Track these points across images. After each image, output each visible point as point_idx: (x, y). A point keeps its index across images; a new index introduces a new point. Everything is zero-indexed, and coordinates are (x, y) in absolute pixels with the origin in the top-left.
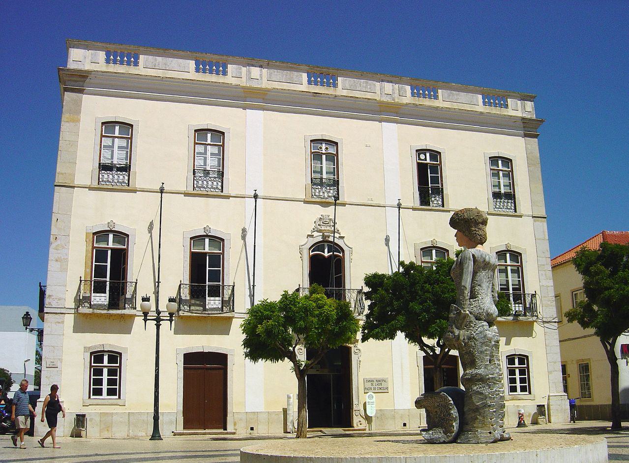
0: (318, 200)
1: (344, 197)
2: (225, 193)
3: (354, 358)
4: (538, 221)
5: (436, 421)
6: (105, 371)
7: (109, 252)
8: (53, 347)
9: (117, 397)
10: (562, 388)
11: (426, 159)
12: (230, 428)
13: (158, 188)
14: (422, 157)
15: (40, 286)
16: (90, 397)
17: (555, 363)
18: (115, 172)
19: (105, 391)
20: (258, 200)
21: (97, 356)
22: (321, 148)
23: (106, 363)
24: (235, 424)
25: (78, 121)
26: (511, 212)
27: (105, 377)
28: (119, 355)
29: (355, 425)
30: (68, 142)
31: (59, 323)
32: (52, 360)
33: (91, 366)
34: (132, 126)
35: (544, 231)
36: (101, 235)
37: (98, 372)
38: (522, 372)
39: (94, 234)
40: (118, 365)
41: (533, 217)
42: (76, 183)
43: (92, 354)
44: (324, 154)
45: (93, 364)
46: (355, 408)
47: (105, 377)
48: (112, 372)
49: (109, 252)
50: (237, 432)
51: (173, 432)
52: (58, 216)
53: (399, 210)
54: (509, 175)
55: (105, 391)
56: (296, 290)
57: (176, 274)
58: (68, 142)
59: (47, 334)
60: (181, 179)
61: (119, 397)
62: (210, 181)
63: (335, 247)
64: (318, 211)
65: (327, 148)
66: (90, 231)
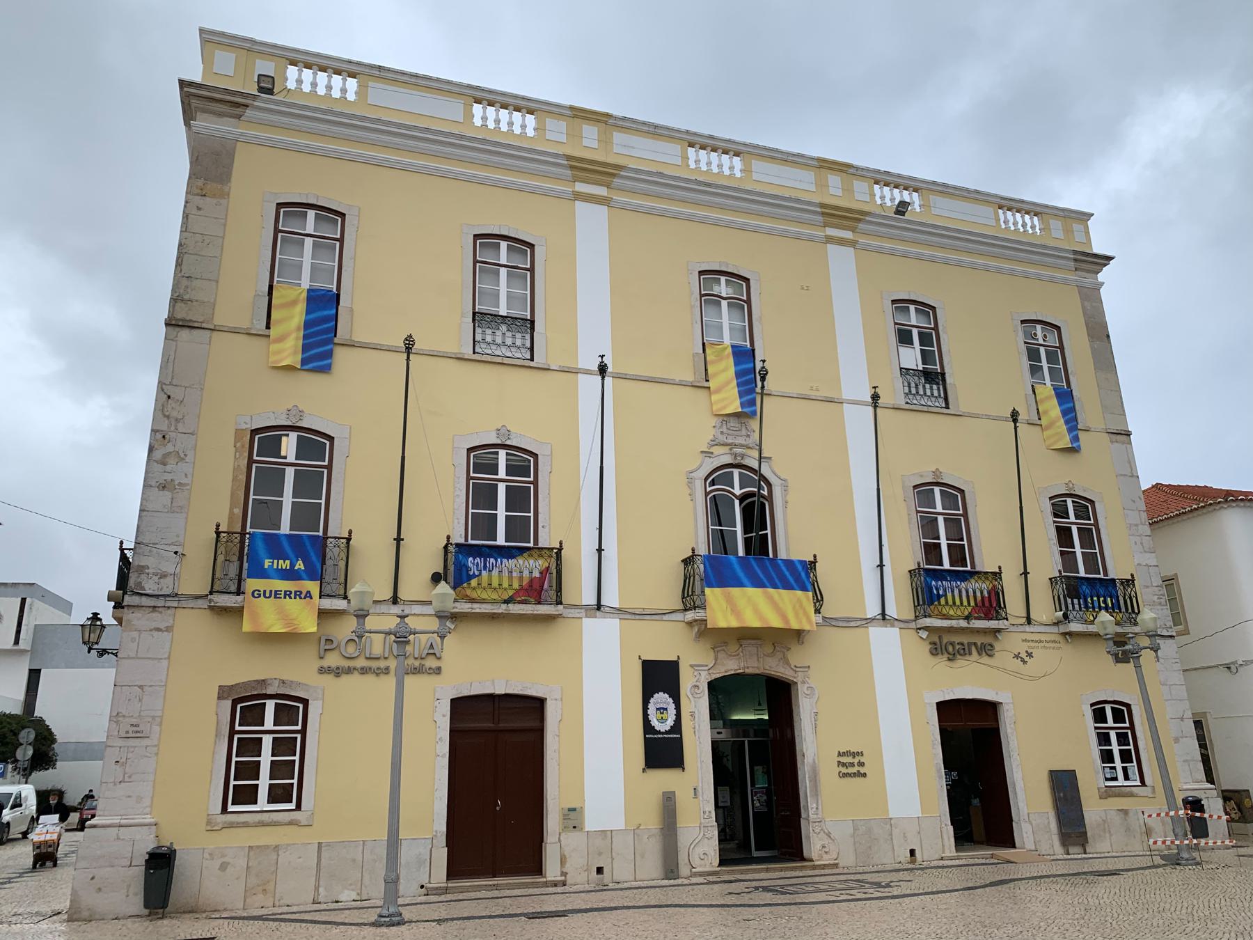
5: (964, 837)
6: (267, 742)
8: (141, 687)
10: (1201, 774)
12: (552, 870)
15: (122, 550)
16: (224, 809)
17: (1182, 719)
19: (263, 794)
21: (246, 704)
23: (269, 723)
24: (563, 861)
25: (225, 195)
27: (266, 759)
28: (301, 706)
30: (199, 238)
31: (158, 630)
32: (134, 721)
34: (343, 215)
37: (252, 746)
38: (1122, 739)
39: (254, 432)
40: (1127, 725)
42: (219, 321)
43: (235, 703)
45: (237, 728)
48: (281, 745)
51: (422, 887)
53: (603, 378)
55: (263, 794)
57: (441, 516)
58: (199, 238)
59: (129, 658)
61: (299, 807)
62: (505, 331)
66: (244, 426)
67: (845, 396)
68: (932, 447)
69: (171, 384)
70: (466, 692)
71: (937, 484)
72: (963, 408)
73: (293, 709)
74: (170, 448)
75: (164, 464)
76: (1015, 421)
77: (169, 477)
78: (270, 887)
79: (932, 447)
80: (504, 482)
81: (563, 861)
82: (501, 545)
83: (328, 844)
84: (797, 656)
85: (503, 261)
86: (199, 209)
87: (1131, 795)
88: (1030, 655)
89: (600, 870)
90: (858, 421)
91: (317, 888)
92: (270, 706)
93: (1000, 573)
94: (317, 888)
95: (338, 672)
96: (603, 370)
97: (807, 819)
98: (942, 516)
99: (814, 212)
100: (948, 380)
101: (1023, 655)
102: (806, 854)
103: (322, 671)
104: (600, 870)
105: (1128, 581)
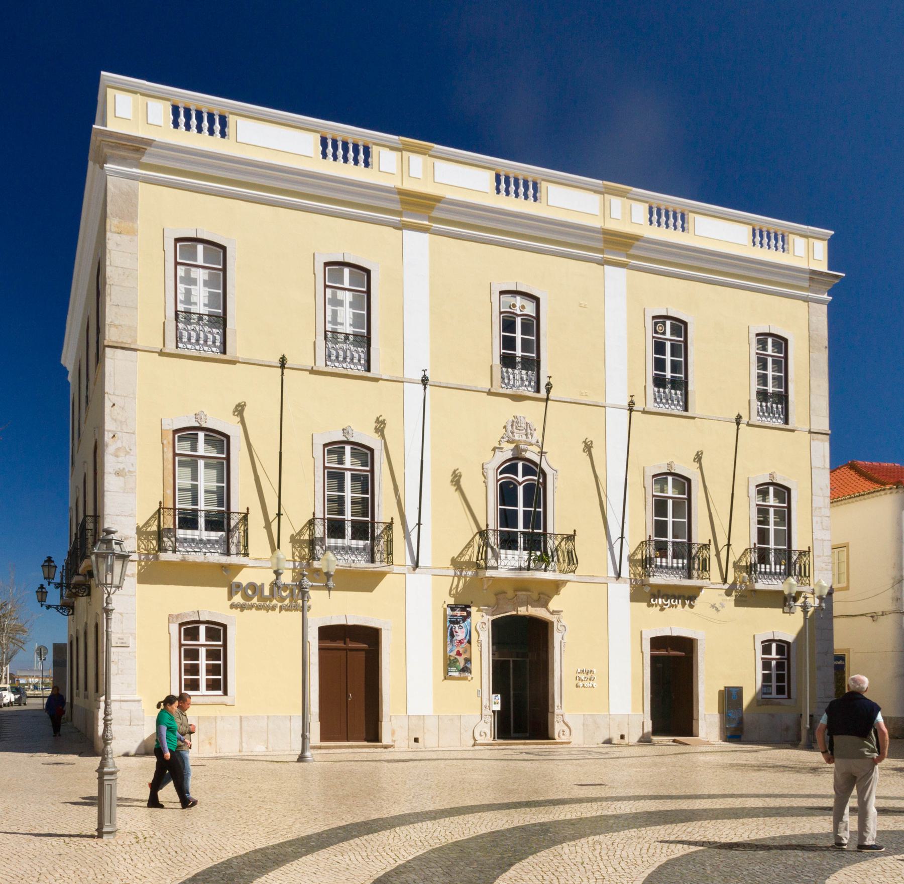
0: (509, 391)
1: (235, 348)
2: (375, 372)
3: (557, 637)
4: (817, 439)
6: (203, 652)
7: (670, 502)
9: (786, 696)
11: (664, 333)
12: (386, 739)
13: (419, 377)
14: (659, 328)
18: (209, 329)
19: (203, 685)
20: (285, 371)
22: (514, 306)
24: (393, 733)
25: (133, 232)
26: (359, 370)
27: (203, 662)
29: (556, 736)
32: (119, 636)
33: (181, 645)
35: (824, 457)
36: (335, 449)
37: (192, 654)
41: (810, 432)
42: (140, 344)
43: (181, 625)
44: (518, 315)
46: (557, 711)
47: (203, 662)
48: (212, 654)
49: (670, 502)
50: (396, 745)
52: (114, 399)
53: (425, 388)
54: (782, 364)
55: (203, 685)
56: (310, 521)
57: (305, 501)
60: (305, 348)
61: (225, 693)
63: (532, 468)
64: (508, 410)
65: (523, 307)
67: (609, 401)
68: (669, 443)
69: (114, 394)
70: (328, 623)
71: (671, 474)
72: (241, 355)
73: (217, 631)
74: (119, 444)
75: (117, 456)
76: (738, 424)
77: (121, 466)
78: (213, 741)
79: (669, 443)
80: (352, 470)
81: (393, 733)
82: (354, 515)
83: (246, 717)
84: (552, 605)
85: (346, 284)
86: (117, 245)
87: (779, 704)
88: (723, 606)
89: (416, 740)
90: (618, 419)
91: (241, 743)
92: (202, 629)
93: (809, 551)
94: (241, 743)
95: (242, 608)
96: (425, 381)
97: (553, 712)
98: (673, 498)
99: (392, 201)
100: (690, 388)
101: (718, 605)
102: (550, 735)
103: (233, 606)
104: (416, 740)
105: (805, 552)
